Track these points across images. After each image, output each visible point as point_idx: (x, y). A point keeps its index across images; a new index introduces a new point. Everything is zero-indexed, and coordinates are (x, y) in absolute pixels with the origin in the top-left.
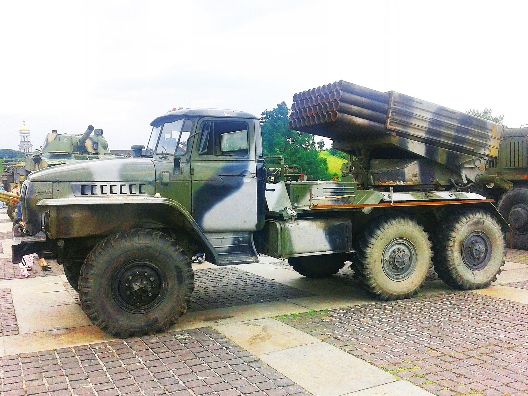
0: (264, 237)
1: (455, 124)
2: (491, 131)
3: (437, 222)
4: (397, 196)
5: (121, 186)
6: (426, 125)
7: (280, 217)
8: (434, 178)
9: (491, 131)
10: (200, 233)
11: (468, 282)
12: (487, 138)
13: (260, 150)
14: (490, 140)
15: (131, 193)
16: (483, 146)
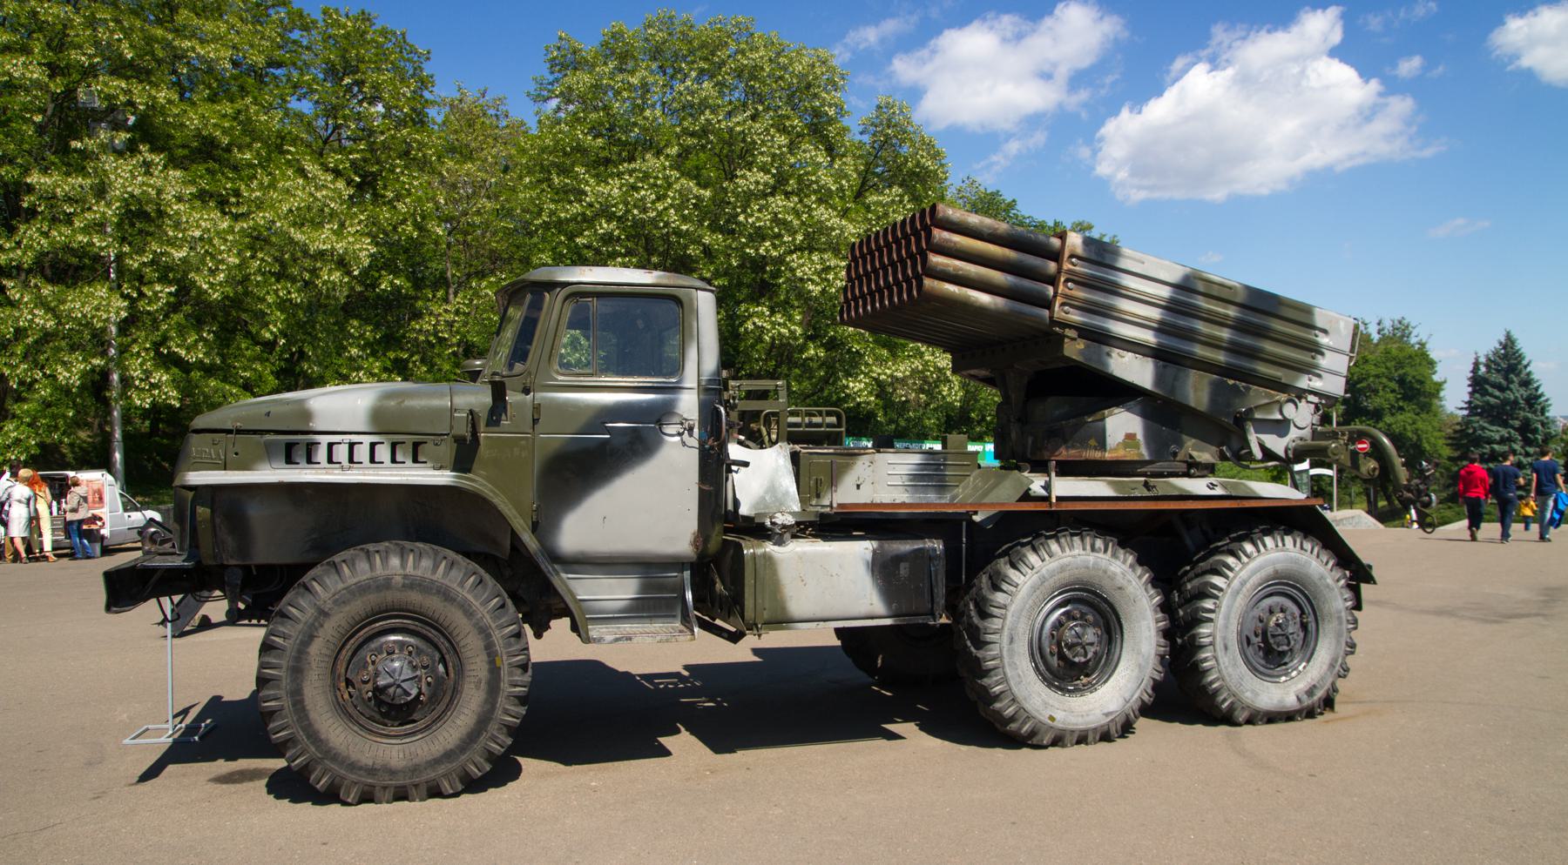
0: (717, 571)
1: (1232, 312)
2: (1325, 331)
3: (1179, 548)
4: (1065, 487)
5: (373, 445)
6: (1155, 314)
7: (758, 529)
8: (1180, 444)
9: (1325, 331)
10: (546, 566)
11: (1022, 714)
12: (1316, 349)
13: (711, 361)
14: (1322, 354)
15: (394, 461)
16: (1309, 369)
